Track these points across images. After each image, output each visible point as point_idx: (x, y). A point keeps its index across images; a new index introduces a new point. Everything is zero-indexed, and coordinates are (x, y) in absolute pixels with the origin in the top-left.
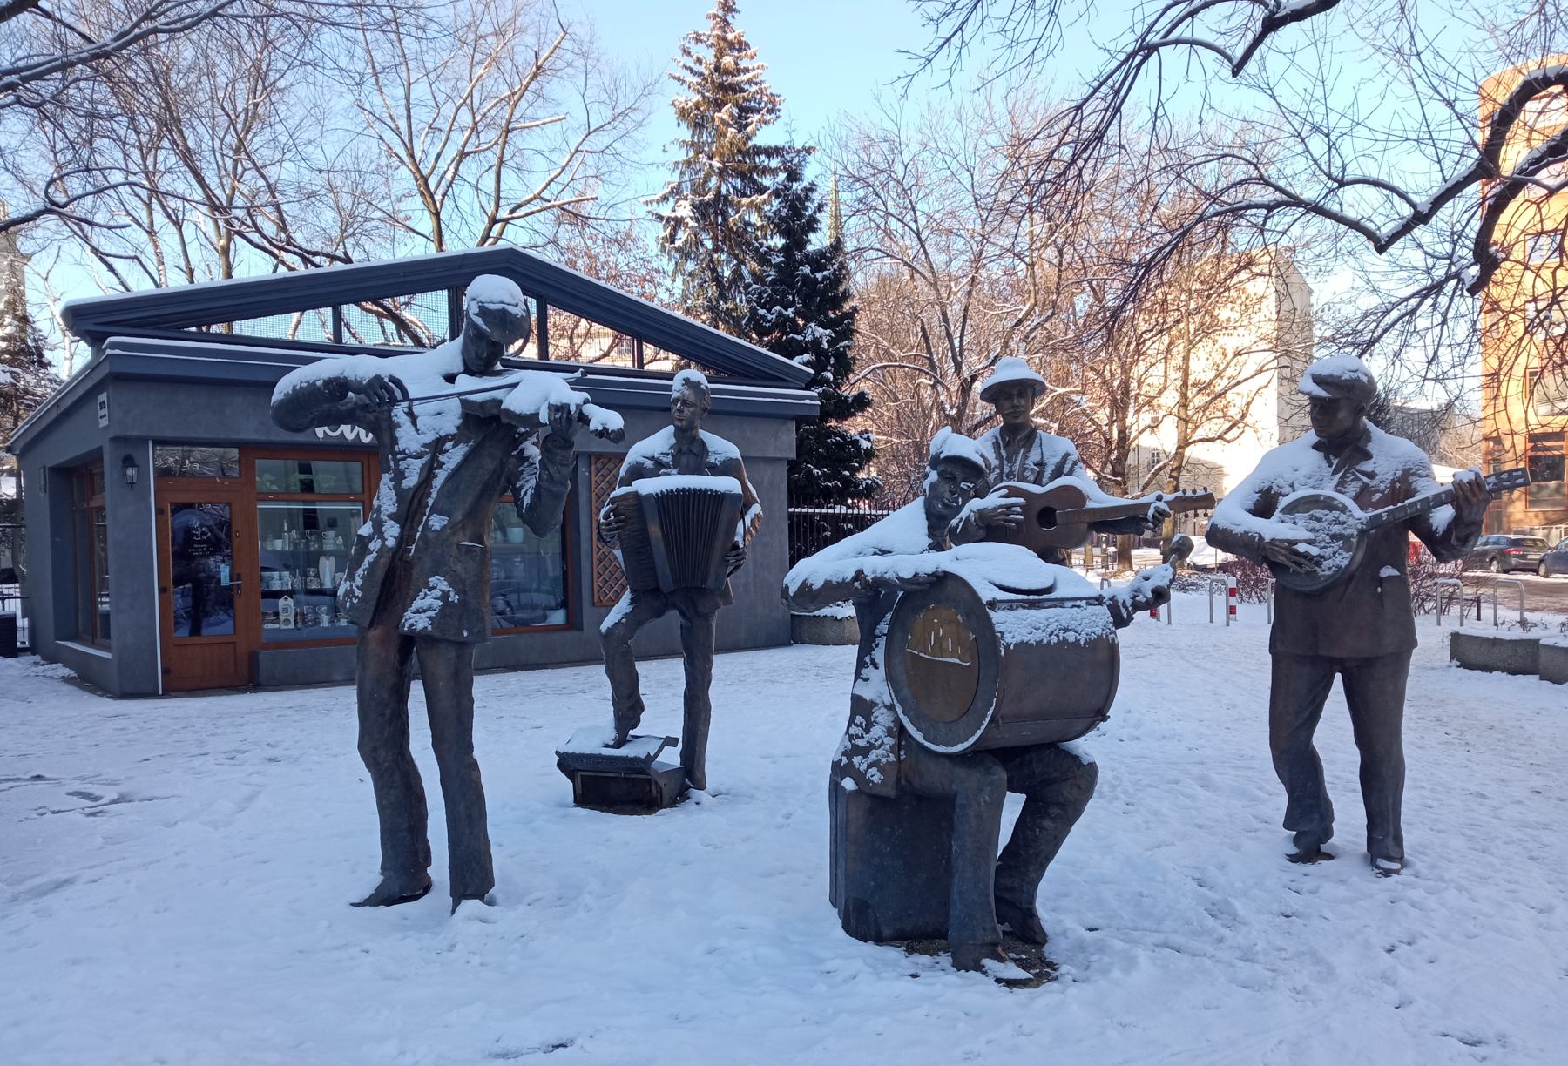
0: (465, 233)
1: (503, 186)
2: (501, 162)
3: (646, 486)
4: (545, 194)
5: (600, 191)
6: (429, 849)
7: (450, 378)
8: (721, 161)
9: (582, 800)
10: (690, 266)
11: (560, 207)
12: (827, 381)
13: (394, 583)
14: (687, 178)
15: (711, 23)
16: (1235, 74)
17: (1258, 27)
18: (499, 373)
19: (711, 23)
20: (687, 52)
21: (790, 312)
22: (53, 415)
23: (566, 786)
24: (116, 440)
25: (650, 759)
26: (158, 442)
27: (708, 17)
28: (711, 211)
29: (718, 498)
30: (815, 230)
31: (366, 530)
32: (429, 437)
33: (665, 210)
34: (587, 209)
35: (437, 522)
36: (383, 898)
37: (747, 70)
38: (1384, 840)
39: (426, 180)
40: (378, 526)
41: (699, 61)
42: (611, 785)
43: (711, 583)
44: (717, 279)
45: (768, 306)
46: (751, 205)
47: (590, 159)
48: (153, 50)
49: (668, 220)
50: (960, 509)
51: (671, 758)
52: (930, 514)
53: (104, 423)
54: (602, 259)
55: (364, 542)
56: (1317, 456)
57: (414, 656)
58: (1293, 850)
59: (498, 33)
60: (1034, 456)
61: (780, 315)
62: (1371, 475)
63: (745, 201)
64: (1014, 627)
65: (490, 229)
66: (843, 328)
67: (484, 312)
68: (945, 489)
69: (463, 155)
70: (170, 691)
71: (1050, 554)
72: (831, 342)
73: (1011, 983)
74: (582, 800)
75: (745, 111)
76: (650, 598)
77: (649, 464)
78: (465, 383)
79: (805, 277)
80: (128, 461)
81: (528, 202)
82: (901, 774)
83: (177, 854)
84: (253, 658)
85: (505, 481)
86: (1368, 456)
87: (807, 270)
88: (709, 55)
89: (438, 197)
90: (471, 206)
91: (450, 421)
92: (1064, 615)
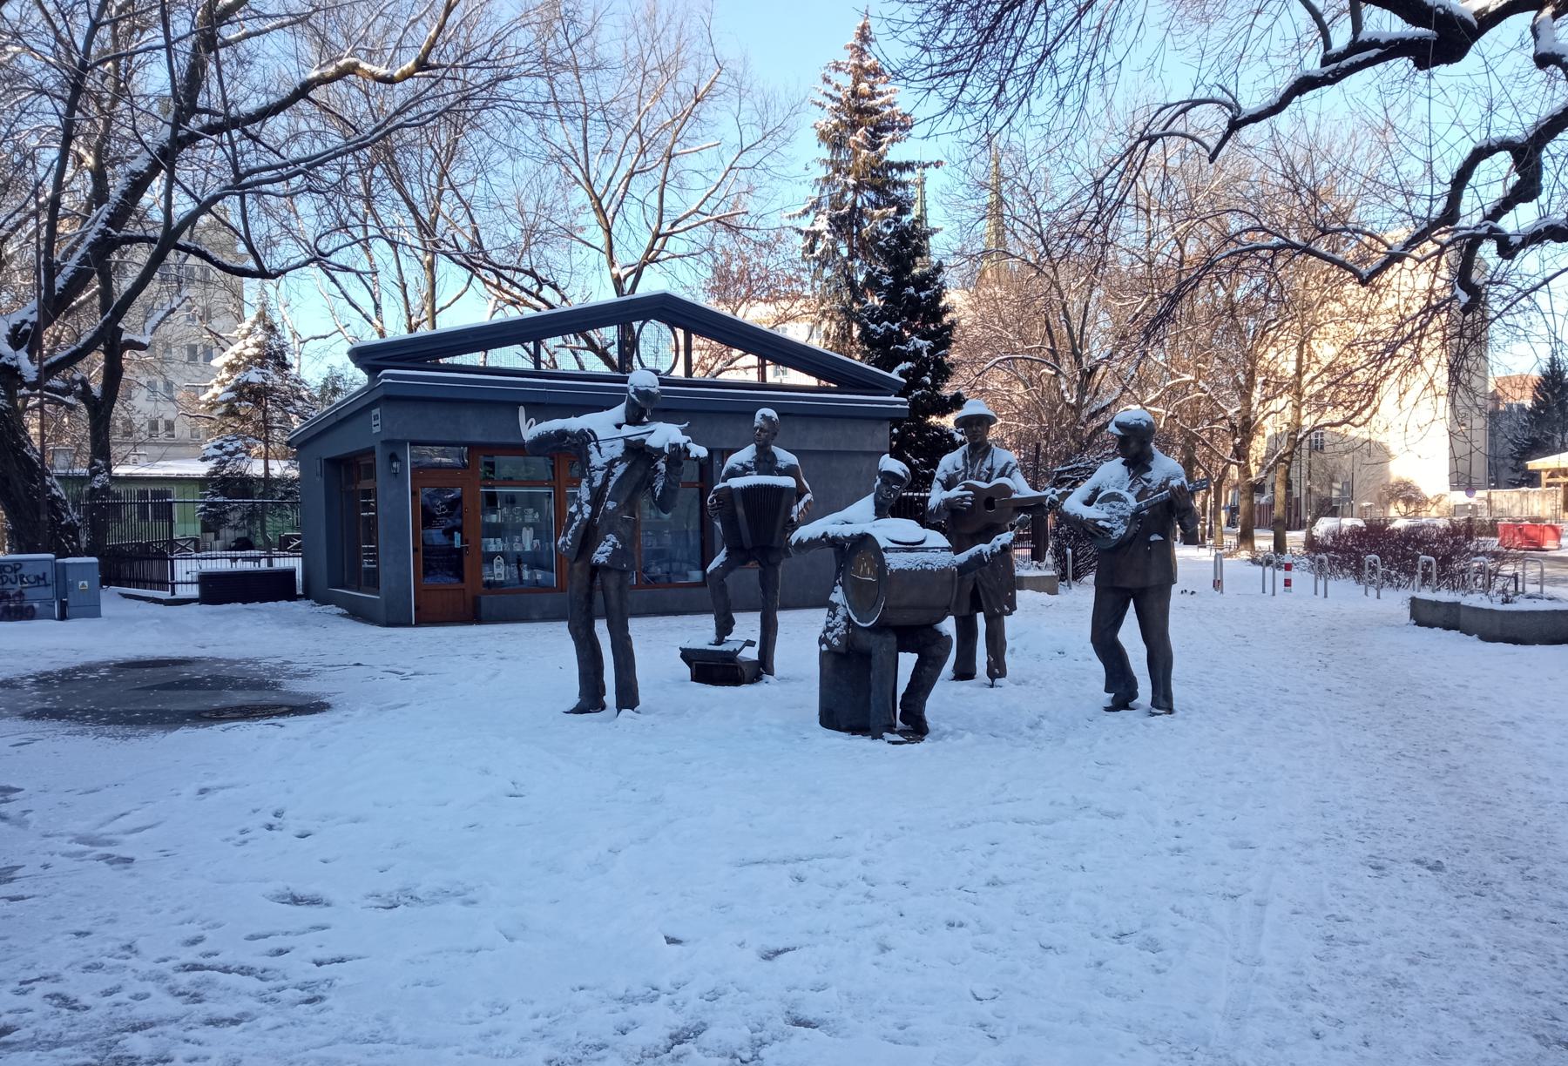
0: (632, 244)
1: (665, 205)
2: (664, 182)
3: (735, 483)
4: (704, 208)
5: (752, 205)
6: (604, 687)
7: (619, 426)
8: (857, 178)
9: (697, 677)
10: (827, 273)
11: (717, 220)
12: (925, 385)
13: (588, 538)
14: (826, 193)
15: (849, 52)
16: (1211, 161)
17: (1225, 127)
18: (644, 424)
19: (849, 52)
20: (827, 80)
21: (896, 327)
22: (333, 421)
23: (686, 671)
24: (385, 443)
25: (736, 652)
26: (413, 444)
27: (846, 48)
28: (845, 223)
29: (780, 490)
30: (921, 255)
31: (573, 509)
32: (607, 459)
33: (805, 224)
34: (742, 220)
35: (611, 505)
36: (579, 710)
37: (880, 94)
38: (1163, 700)
39: (599, 201)
40: (580, 507)
41: (838, 88)
42: (713, 668)
43: (776, 543)
44: (851, 284)
45: (877, 322)
46: (883, 217)
47: (743, 175)
49: (807, 234)
51: (751, 654)
52: (876, 503)
53: (377, 430)
54: (755, 260)
55: (572, 515)
56: (1124, 468)
57: (598, 580)
58: (1109, 704)
59: (663, 68)
60: (987, 464)
61: (888, 328)
62: (1149, 481)
63: (877, 213)
64: (896, 561)
65: (654, 243)
66: (942, 338)
67: (637, 392)
68: (884, 489)
69: (631, 174)
70: (421, 622)
72: (931, 351)
73: (894, 743)
74: (697, 677)
75: (878, 130)
76: (739, 555)
77: (739, 468)
78: (628, 430)
79: (910, 296)
80: (393, 458)
81: (686, 217)
82: (848, 640)
83: (375, 804)
84: (476, 602)
85: (648, 483)
86: (1149, 469)
87: (911, 290)
88: (846, 81)
89: (609, 214)
90: (638, 219)
91: (618, 450)
92: (926, 556)
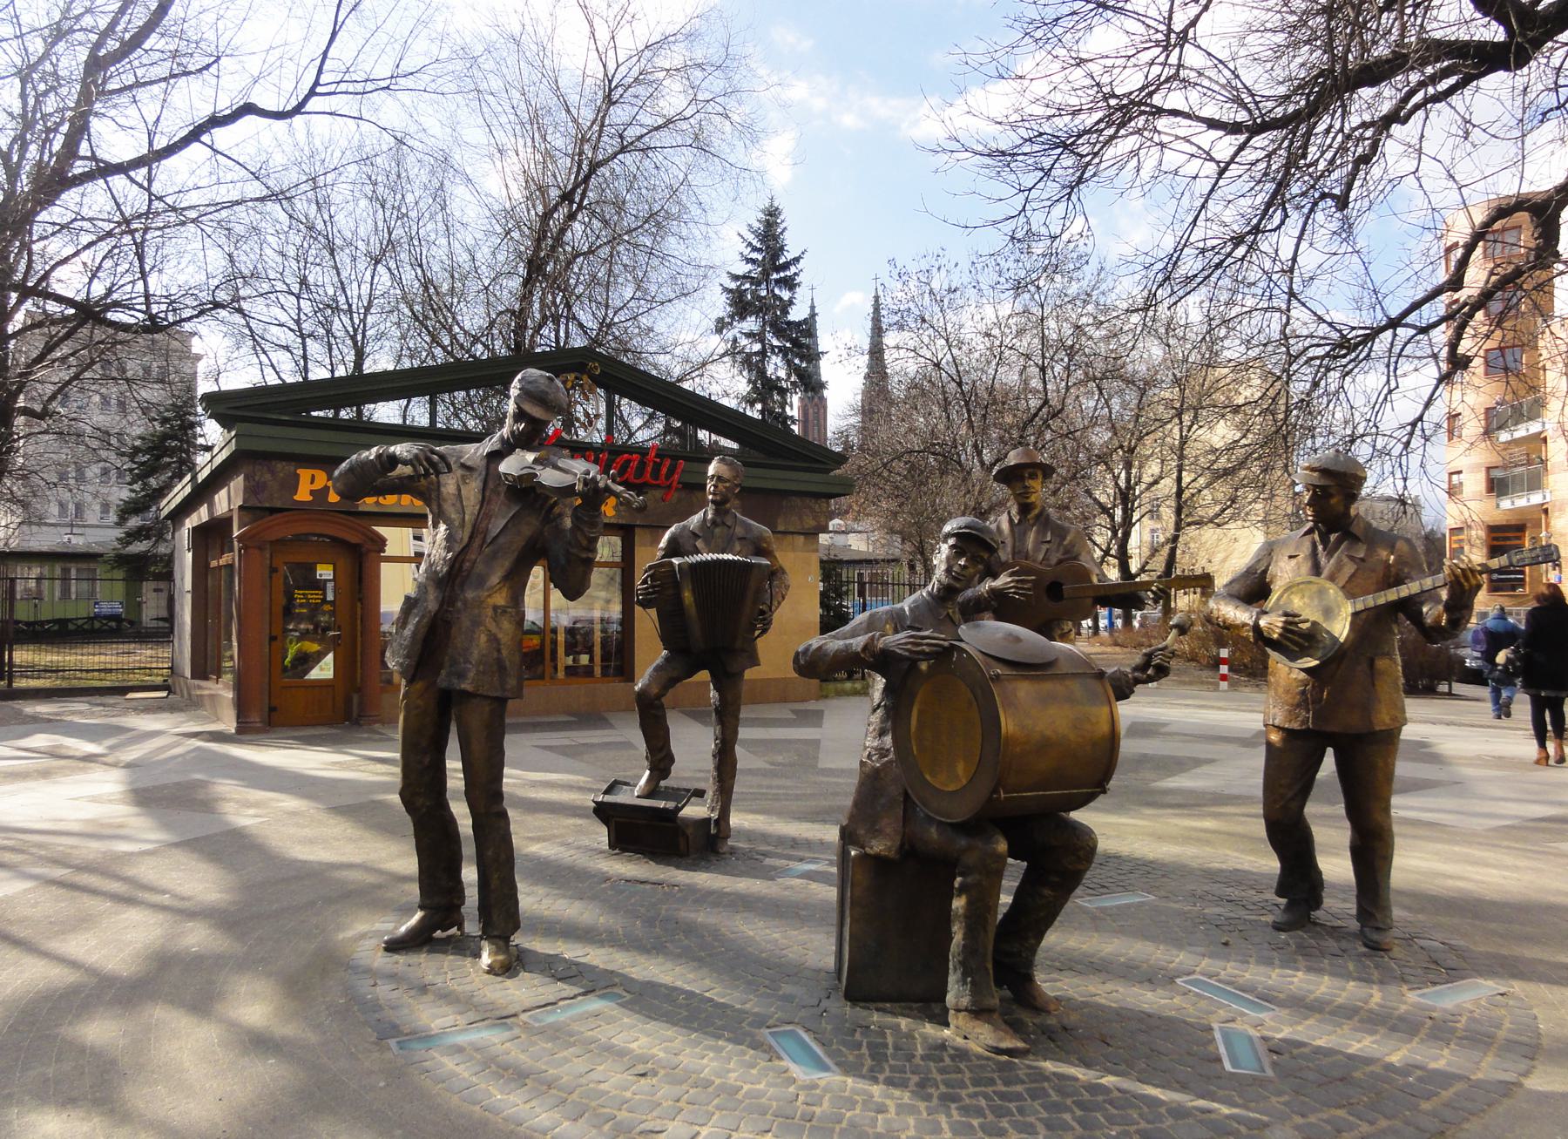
6: (463, 890)
48: (893, 505)
50: (698, 552)
71: (1047, 629)
